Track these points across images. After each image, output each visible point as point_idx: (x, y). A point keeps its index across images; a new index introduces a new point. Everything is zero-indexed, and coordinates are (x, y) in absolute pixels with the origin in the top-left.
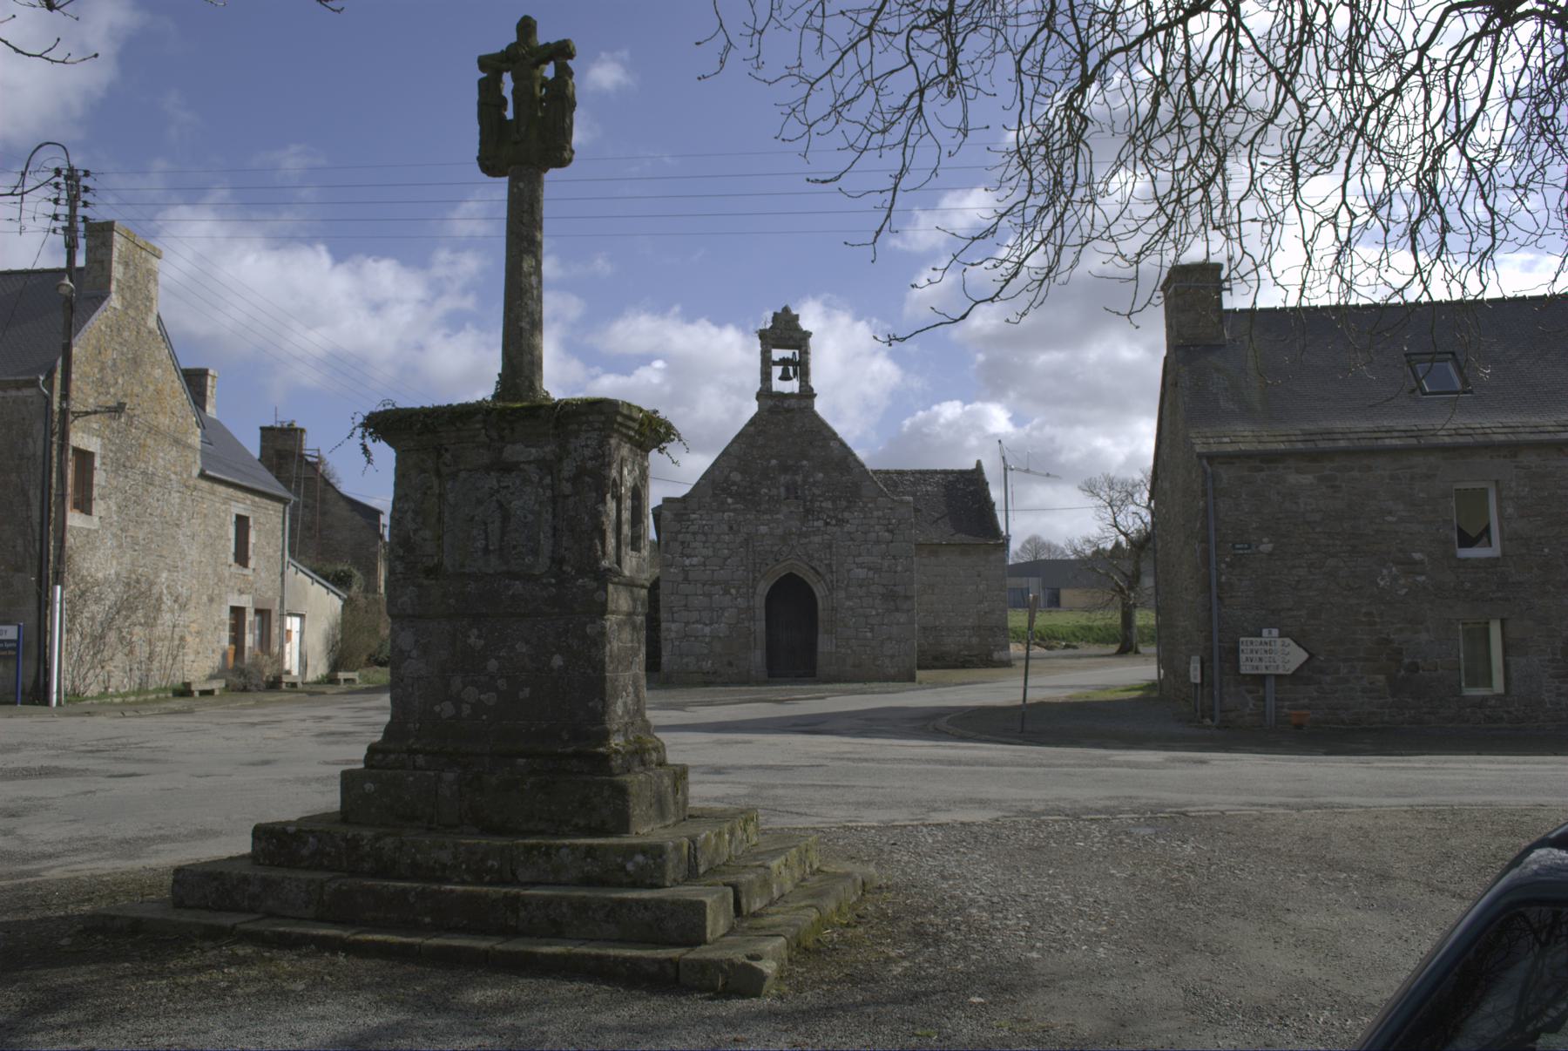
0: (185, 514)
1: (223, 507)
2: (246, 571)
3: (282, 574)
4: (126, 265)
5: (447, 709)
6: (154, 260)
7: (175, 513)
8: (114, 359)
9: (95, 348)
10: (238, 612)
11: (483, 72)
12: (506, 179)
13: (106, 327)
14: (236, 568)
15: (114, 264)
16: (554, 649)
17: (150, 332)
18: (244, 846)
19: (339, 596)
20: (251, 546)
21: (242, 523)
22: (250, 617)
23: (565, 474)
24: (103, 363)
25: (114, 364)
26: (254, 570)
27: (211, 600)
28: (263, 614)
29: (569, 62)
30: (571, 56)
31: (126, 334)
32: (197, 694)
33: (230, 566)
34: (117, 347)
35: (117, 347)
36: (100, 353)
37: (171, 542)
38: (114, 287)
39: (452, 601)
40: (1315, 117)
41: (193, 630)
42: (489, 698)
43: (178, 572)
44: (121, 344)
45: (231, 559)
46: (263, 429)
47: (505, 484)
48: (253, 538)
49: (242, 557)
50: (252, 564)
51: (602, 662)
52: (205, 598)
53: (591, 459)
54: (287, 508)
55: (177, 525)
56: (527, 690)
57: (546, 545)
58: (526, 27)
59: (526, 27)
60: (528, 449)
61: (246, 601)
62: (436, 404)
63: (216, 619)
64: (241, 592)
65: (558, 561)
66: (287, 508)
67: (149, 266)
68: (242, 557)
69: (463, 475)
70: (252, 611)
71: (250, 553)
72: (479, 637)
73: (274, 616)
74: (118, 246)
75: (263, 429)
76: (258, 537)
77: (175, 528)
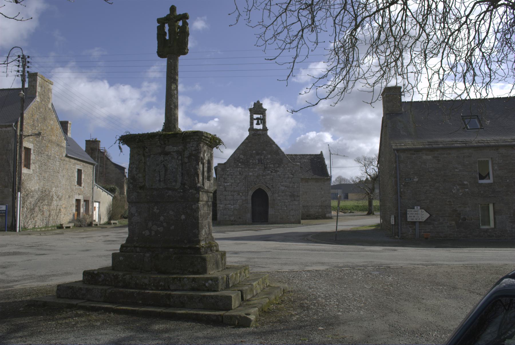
0: (61, 169)
1: (73, 167)
2: (81, 188)
3: (93, 188)
4: (42, 87)
5: (147, 233)
6: (51, 85)
7: (57, 168)
8: (37, 118)
9: (31, 114)
10: (78, 201)
11: (159, 24)
12: (166, 59)
13: (35, 107)
14: (77, 187)
15: (38, 87)
16: (182, 213)
17: (49, 109)
18: (80, 278)
19: (111, 196)
20: (82, 179)
21: (79, 172)
22: (82, 203)
23: (186, 156)
24: (34, 119)
25: (38, 120)
26: (83, 187)
27: (69, 197)
28: (86, 201)
29: (187, 20)
30: (187, 18)
31: (41, 110)
32: (65, 228)
33: (76, 186)
34: (38, 114)
35: (38, 114)
36: (33, 116)
37: (56, 178)
38: (37, 94)
39: (148, 197)
40: (432, 38)
41: (63, 207)
42: (161, 229)
43: (58, 188)
44: (40, 113)
45: (76, 184)
46: (86, 141)
47: (166, 159)
48: (83, 177)
49: (79, 183)
50: (83, 185)
51: (198, 217)
52: (67, 196)
53: (194, 151)
54: (94, 167)
55: (58, 172)
56: (173, 227)
57: (179, 179)
58: (173, 9)
59: (173, 9)
60: (174, 147)
61: (81, 197)
62: (143, 133)
63: (71, 203)
64: (79, 194)
65: (183, 184)
66: (94, 167)
67: (49, 87)
68: (79, 183)
69: (152, 156)
70: (83, 201)
71: (82, 181)
72: (157, 209)
73: (90, 202)
74: (39, 81)
75: (86, 141)
76: (85, 176)
77: (57, 173)
